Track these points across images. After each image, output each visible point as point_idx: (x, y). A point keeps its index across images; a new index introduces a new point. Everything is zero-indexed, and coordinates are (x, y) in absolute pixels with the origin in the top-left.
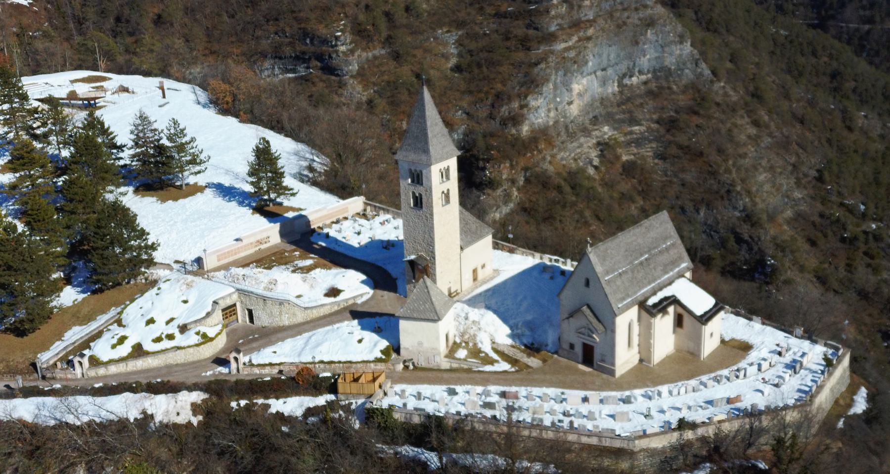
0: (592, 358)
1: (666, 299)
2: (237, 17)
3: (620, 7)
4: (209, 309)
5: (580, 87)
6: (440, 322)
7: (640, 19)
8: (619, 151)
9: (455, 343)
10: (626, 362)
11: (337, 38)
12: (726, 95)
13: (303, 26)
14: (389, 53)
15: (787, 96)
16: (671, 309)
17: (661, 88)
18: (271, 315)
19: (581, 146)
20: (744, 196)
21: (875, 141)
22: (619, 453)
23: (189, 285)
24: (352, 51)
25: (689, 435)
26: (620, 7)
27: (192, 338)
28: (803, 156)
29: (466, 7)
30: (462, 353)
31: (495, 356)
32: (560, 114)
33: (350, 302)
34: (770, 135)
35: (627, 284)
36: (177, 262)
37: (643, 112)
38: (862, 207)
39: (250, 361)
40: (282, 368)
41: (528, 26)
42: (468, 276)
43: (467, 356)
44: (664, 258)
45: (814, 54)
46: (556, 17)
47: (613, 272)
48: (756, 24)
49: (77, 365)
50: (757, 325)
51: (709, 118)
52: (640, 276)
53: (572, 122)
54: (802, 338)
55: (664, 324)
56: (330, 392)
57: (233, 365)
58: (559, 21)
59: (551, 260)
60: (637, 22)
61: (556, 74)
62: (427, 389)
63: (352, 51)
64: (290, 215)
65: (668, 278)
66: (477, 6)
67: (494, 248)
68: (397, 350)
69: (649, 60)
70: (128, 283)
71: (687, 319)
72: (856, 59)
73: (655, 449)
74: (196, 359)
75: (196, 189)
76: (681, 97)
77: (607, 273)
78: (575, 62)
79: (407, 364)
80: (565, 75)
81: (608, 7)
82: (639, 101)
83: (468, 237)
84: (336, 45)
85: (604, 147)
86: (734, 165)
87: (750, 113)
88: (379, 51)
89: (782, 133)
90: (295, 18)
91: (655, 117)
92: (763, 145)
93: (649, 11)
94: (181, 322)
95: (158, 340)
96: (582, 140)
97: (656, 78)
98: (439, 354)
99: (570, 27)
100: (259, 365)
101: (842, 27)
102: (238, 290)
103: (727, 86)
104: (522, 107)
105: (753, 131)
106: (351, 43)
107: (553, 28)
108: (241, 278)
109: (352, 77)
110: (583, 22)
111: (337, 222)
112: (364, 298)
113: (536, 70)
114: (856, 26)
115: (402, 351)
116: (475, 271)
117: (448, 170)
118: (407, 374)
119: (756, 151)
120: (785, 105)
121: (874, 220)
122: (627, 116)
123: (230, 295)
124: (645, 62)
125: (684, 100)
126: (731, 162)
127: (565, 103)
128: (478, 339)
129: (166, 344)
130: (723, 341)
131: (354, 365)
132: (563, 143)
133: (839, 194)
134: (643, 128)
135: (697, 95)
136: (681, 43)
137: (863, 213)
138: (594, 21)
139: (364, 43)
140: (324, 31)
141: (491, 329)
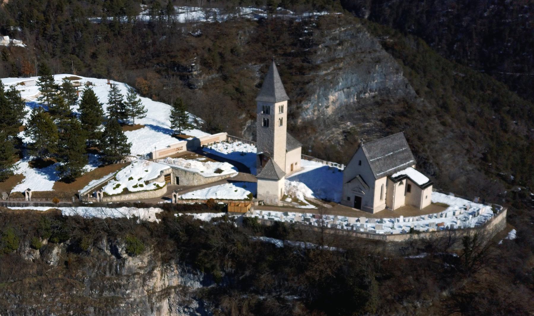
0: (361, 204)
1: (401, 176)
2: (136, 55)
3: (360, 51)
4: (159, 174)
5: (334, 98)
6: (279, 181)
7: (372, 58)
8: (356, 137)
9: (284, 195)
10: (379, 207)
11: (192, 67)
12: (424, 106)
13: (173, 60)
14: (221, 77)
15: (464, 109)
16: (404, 181)
17: (384, 100)
18: (188, 180)
19: (333, 133)
20: (434, 166)
21: (522, 139)
22: (377, 243)
23: (147, 164)
24: (200, 75)
25: (416, 237)
26: (360, 51)
27: (152, 187)
28: (474, 144)
29: (266, 50)
30: (289, 200)
31: (307, 202)
32: (321, 113)
33: (227, 176)
34: (452, 131)
35: (382, 165)
36: (138, 155)
37: (372, 114)
38: (512, 177)
39: (181, 198)
40: (197, 201)
41: (303, 61)
42: (288, 167)
43: (291, 201)
44: (401, 156)
45: (482, 88)
46: (320, 55)
47: (374, 158)
48: (443, 69)
49: (98, 195)
50: (452, 197)
51: (414, 119)
52: (388, 162)
53: (328, 118)
54: (479, 203)
55: (400, 189)
56: (223, 212)
57: (174, 199)
58: (322, 58)
59: (332, 165)
60: (370, 60)
61: (319, 89)
62: (273, 213)
63: (200, 75)
64: (190, 139)
65: (403, 166)
66: (273, 49)
67: (302, 158)
68: (255, 196)
69: (376, 83)
70: (116, 163)
71: (413, 188)
72: (510, 93)
73: (397, 242)
74: (153, 197)
75: (139, 127)
76: (396, 106)
77: (371, 158)
78: (331, 82)
79: (260, 203)
80: (325, 90)
81: (352, 51)
82: (370, 107)
83: (290, 146)
84: (192, 71)
85: (347, 134)
86: (428, 147)
87: (439, 117)
88: (215, 75)
89: (460, 130)
90: (169, 56)
91: (379, 117)
92: (447, 137)
93: (378, 54)
94: (146, 179)
95: (135, 187)
96: (334, 129)
97: (381, 94)
98: (278, 198)
99: (329, 62)
100: (186, 200)
101: (501, 74)
102: (171, 167)
103: (425, 101)
104: (298, 108)
105: (441, 128)
106: (200, 70)
107: (319, 62)
108: (173, 162)
109: (199, 89)
110: (337, 59)
111: (215, 143)
112: (234, 175)
113: (307, 86)
114: (511, 73)
115: (258, 196)
116: (292, 165)
117: (282, 107)
118: (261, 207)
119: (443, 140)
120: (463, 114)
121: (520, 185)
122: (362, 116)
123: (168, 169)
124: (374, 84)
125: (398, 108)
126: (426, 146)
127: (324, 107)
128: (297, 194)
129: (139, 189)
130: (432, 203)
131: (234, 202)
132: (322, 130)
133: (497, 169)
134: (371, 124)
135: (406, 105)
136: (397, 73)
137: (513, 181)
138: (344, 58)
139: (207, 70)
140: (185, 63)
141: (303, 190)
